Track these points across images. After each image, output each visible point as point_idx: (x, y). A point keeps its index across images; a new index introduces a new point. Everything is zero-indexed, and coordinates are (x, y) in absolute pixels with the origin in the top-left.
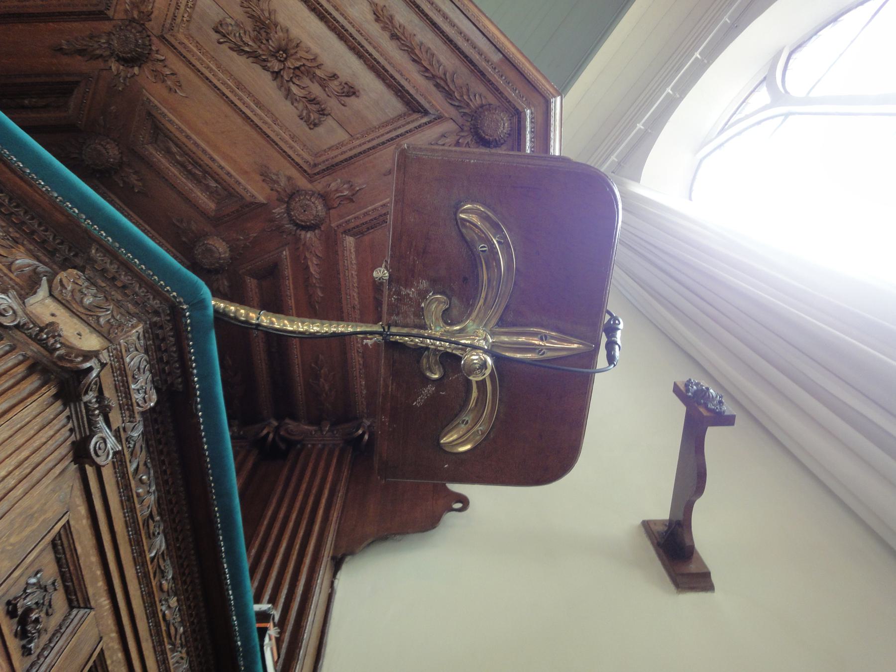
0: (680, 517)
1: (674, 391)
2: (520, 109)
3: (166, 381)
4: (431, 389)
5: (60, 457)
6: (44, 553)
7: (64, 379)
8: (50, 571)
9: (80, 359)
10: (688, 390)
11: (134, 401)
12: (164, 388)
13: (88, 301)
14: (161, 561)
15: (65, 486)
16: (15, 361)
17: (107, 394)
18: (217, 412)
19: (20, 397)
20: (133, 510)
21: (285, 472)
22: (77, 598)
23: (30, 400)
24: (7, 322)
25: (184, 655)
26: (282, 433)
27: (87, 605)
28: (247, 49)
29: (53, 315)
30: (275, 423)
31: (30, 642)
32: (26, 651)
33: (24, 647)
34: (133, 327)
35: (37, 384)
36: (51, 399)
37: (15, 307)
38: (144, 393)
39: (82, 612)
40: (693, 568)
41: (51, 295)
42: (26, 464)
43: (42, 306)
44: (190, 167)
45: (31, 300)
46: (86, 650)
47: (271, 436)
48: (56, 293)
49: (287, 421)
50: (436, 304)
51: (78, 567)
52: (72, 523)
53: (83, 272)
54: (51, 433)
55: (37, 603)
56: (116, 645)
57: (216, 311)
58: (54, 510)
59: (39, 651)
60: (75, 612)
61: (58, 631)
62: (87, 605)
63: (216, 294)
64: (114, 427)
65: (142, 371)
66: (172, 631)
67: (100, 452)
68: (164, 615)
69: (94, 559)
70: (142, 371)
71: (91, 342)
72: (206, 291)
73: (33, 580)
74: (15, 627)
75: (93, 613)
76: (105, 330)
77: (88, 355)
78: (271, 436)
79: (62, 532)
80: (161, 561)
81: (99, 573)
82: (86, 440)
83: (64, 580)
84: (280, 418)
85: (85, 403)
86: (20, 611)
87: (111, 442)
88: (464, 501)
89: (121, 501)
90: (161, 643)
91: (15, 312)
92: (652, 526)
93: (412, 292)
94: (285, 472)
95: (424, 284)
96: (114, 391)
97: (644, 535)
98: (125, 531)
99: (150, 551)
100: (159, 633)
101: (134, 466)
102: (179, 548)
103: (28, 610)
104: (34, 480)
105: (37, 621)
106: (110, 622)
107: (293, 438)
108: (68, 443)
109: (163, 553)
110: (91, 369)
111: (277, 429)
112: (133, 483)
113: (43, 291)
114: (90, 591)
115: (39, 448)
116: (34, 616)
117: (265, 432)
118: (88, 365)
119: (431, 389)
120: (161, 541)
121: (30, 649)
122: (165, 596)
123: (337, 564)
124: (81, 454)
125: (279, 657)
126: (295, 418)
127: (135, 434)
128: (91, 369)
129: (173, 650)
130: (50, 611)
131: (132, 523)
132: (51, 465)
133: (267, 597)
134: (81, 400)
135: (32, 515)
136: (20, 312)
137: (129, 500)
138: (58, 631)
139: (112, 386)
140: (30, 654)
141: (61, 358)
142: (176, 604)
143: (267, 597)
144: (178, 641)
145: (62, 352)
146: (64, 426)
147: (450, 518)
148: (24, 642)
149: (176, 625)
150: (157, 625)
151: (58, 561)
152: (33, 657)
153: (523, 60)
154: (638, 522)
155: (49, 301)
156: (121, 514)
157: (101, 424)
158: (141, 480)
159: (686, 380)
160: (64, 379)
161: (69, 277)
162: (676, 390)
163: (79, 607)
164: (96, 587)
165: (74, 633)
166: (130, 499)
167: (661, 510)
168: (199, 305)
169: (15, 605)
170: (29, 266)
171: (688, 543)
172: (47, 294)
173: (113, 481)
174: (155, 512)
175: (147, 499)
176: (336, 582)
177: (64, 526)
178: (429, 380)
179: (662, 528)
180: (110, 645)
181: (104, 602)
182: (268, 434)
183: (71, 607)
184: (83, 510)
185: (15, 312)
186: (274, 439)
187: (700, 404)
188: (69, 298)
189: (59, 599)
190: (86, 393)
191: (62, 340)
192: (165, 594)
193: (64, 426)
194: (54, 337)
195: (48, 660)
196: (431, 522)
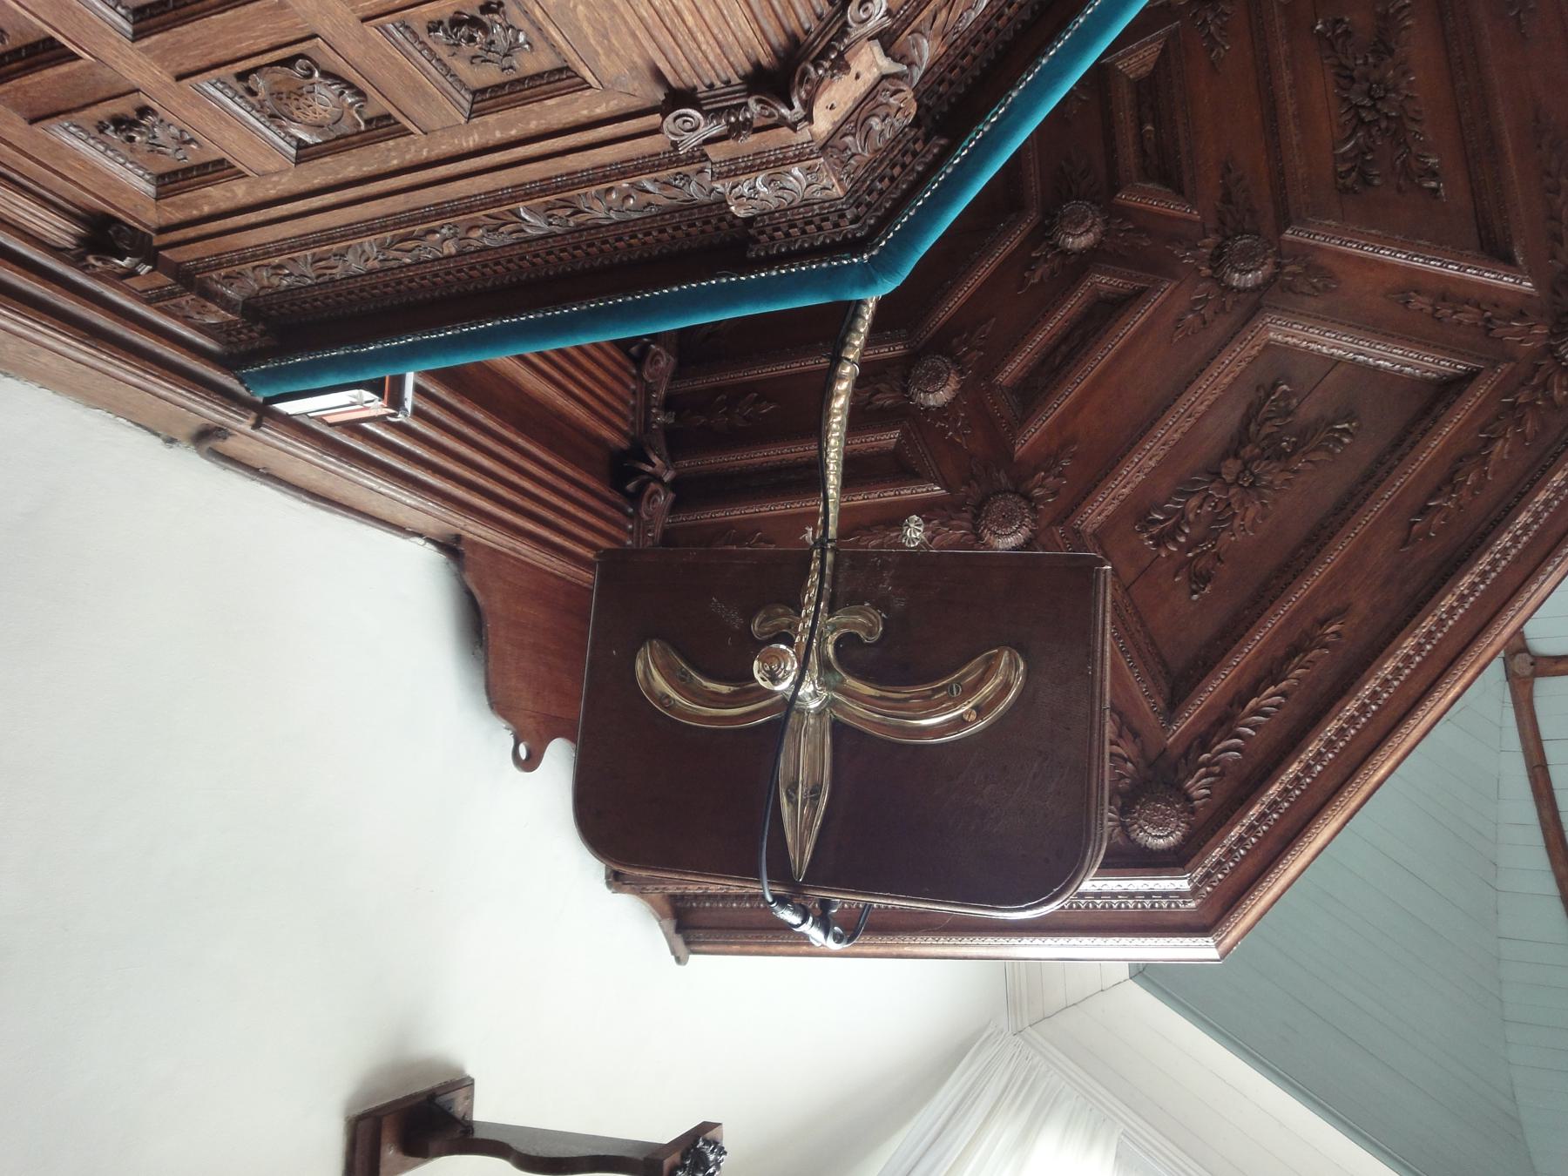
0: (479, 1134)
1: (704, 1123)
2: (1190, 865)
3: (763, 233)
4: (737, 622)
5: (679, 69)
6: (553, 56)
7: (782, 75)
8: (530, 63)
9: (803, 94)
10: (707, 1142)
11: (743, 178)
12: (751, 231)
13: (875, 123)
14: (510, 227)
15: (636, 84)
16: (803, 18)
17: (753, 138)
18: (714, 308)
19: (760, 17)
20: (591, 182)
21: (593, 484)
22: (486, 100)
23: (756, 27)
24: (852, 9)
25: (370, 264)
26: (653, 486)
27: (473, 113)
28: (1253, 428)
29: (857, 77)
30: (667, 478)
31: (445, 31)
32: (433, 27)
33: (441, 23)
34: (840, 180)
35: (774, 40)
36: (753, 59)
37: (870, 24)
38: (752, 195)
39: (466, 105)
40: (389, 1153)
41: (884, 77)
42: (677, 21)
43: (870, 62)
44: (1064, 348)
45: (876, 48)
46: (416, 110)
47: (649, 469)
48: (885, 84)
49: (671, 496)
50: (865, 622)
51: (527, 101)
52: (588, 92)
53: (911, 125)
54: (711, 58)
55: (492, 42)
56: (410, 157)
57: (860, 303)
58: (610, 67)
59: (430, 43)
60: (469, 97)
61: (449, 72)
62: (473, 113)
63: (881, 304)
64: (709, 150)
65: (780, 193)
66: (409, 245)
67: (679, 121)
68: (433, 231)
69: (534, 126)
70: (780, 193)
71: (823, 122)
72: (888, 286)
73: (522, 38)
74: (468, 11)
75: (463, 121)
76: (836, 141)
77: (808, 105)
78: (649, 469)
79: (578, 80)
80: (510, 227)
81: (513, 132)
82: (696, 103)
83: (512, 83)
84: (674, 485)
85: (746, 104)
86: (485, 18)
87: (692, 140)
88: (529, 763)
89: (604, 166)
90: (397, 225)
91: (864, 21)
92: (462, 1093)
93: (887, 587)
94: (593, 484)
95: (899, 604)
96: (755, 149)
97: (448, 1079)
98: (564, 171)
99: (529, 210)
100: (413, 221)
101: (649, 187)
102: (523, 259)
103: (486, 30)
104: (656, 33)
105: (471, 39)
106: (445, 148)
107: (644, 502)
108: (696, 81)
109: (522, 231)
110: (791, 107)
111: (659, 480)
112: (625, 184)
113: (887, 65)
114: (491, 119)
115: (695, 39)
116: (479, 35)
117: (655, 460)
118: (797, 104)
119: (737, 622)
120: (539, 228)
121: (436, 30)
122: (461, 231)
123: (451, 547)
124: (678, 98)
125: (331, 425)
126: (675, 508)
127: (693, 188)
128: (791, 107)
129: (383, 247)
130: (477, 61)
131: (575, 180)
132: (671, 56)
133: (426, 406)
134: (748, 96)
135: (606, 36)
136: (863, 31)
137: (605, 176)
138: (449, 72)
139: (763, 147)
140: (430, 30)
141: (805, 73)
142: (446, 252)
143: (426, 406)
144: (392, 254)
145: (813, 75)
146: (718, 76)
147: (502, 738)
148: (446, 24)
149: (416, 252)
150: (425, 219)
151: (540, 75)
152: (424, 37)
153: (1276, 890)
154: (470, 1071)
155: (875, 73)
156: (587, 165)
157: (716, 129)
158: (629, 196)
159: (726, 1144)
160: (782, 75)
161: (904, 104)
162: (706, 1127)
163: (473, 103)
164: (496, 127)
165: (443, 91)
166: (606, 178)
167: (486, 1110)
168: (867, 278)
169: (495, 11)
170: (921, 57)
171: (434, 1146)
172: (885, 72)
173: (633, 154)
174: (581, 218)
175: (599, 208)
176: (421, 541)
177: (585, 82)
178: (749, 616)
179: (459, 1109)
180: (413, 148)
181: (472, 141)
182: (653, 465)
183: (474, 93)
184: (601, 110)
185: (864, 21)
186: (644, 473)
187: (684, 1157)
188: (881, 99)
189: (490, 75)
190: (758, 101)
191: (826, 82)
192: (461, 235)
193: (718, 76)
194: (832, 68)
195: (417, 54)
196: (500, 703)
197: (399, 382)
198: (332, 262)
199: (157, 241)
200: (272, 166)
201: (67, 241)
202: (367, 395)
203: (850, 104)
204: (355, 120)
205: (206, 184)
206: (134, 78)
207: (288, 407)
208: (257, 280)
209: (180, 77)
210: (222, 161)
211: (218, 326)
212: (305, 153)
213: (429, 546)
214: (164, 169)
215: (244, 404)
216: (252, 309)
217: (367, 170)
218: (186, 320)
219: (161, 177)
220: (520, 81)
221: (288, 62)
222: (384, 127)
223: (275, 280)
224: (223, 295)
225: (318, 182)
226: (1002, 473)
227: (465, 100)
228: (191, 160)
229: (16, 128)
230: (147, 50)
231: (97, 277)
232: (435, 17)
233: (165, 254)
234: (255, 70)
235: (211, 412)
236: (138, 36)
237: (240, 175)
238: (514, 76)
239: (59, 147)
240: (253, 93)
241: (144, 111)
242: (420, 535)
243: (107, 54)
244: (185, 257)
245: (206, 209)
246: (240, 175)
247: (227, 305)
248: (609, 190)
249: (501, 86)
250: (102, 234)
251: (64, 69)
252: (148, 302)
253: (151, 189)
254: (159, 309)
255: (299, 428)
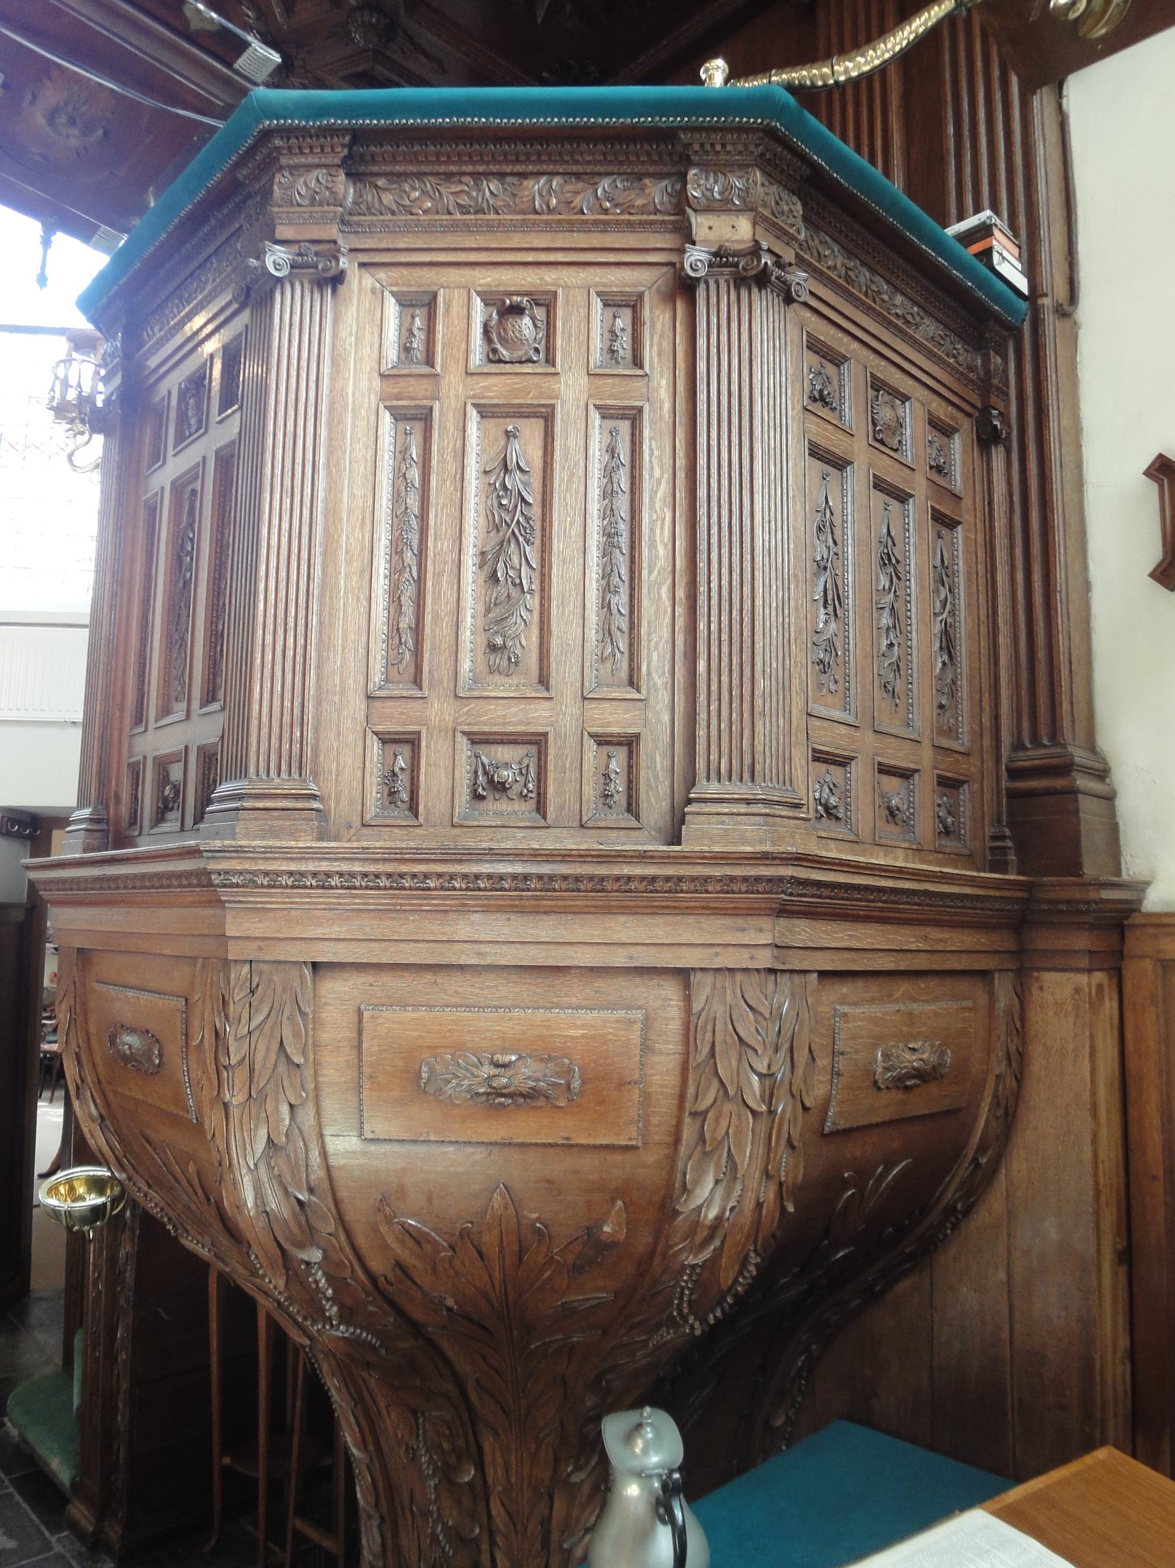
8: (815, 359)
27: (846, 359)
62: (846, 359)
69: (832, 331)
73: (811, 376)
103: (821, 391)
106: (866, 352)
114: (842, 350)
181: (855, 345)
197: (967, 238)
198: (938, 339)
199: (977, 414)
200: (918, 405)
201: (1001, 449)
202: (996, 258)
203: (723, 217)
204: (883, 397)
205: (941, 420)
206: (924, 482)
207: (1022, 284)
208: (963, 354)
209: (913, 470)
210: (929, 424)
211: (998, 353)
212: (905, 398)
213: (1065, 92)
214: (945, 439)
215: (1036, 311)
216: (978, 343)
217: (893, 369)
218: (1006, 370)
219: (948, 437)
220: (823, 357)
221: (882, 442)
222: (878, 385)
223: (961, 351)
224: (982, 365)
225: (911, 382)
226: (166, 794)
227: (845, 368)
228: (935, 433)
229: (967, 502)
230: (913, 489)
231: (1009, 426)
232: (830, 412)
233: (979, 405)
234: (892, 449)
235: (1050, 322)
236: (911, 496)
237: (929, 412)
238: (823, 361)
239: (965, 483)
240: (900, 442)
241: (931, 467)
242: (1060, 106)
243: (923, 498)
244: (976, 397)
245: (950, 409)
246: (929, 412)
247: (986, 360)
248: (829, 268)
249: (829, 361)
250: (987, 438)
251: (937, 506)
252: (1007, 394)
253: (956, 436)
254: (1008, 387)
255: (1031, 269)
